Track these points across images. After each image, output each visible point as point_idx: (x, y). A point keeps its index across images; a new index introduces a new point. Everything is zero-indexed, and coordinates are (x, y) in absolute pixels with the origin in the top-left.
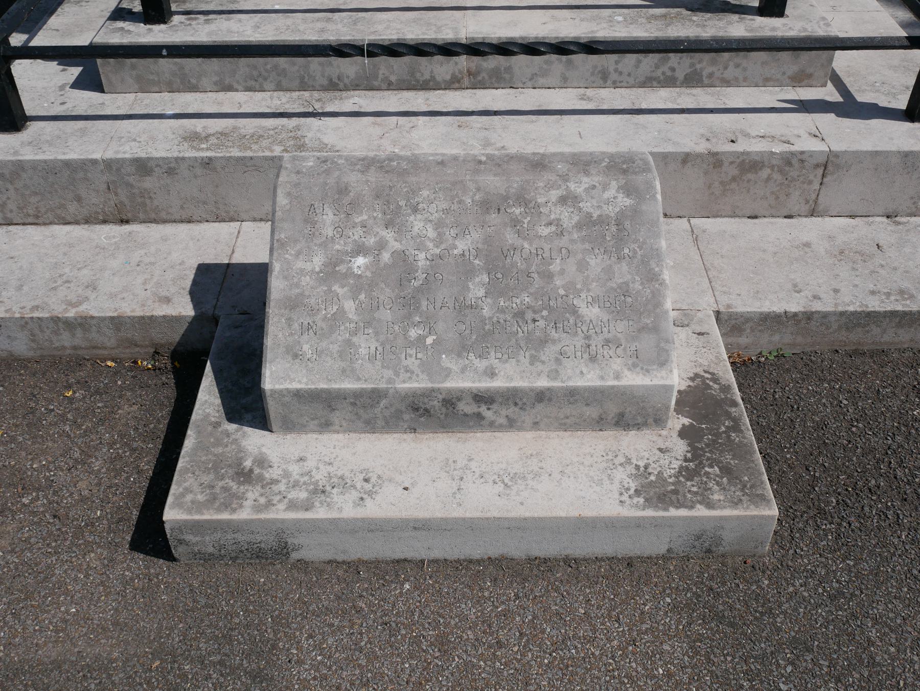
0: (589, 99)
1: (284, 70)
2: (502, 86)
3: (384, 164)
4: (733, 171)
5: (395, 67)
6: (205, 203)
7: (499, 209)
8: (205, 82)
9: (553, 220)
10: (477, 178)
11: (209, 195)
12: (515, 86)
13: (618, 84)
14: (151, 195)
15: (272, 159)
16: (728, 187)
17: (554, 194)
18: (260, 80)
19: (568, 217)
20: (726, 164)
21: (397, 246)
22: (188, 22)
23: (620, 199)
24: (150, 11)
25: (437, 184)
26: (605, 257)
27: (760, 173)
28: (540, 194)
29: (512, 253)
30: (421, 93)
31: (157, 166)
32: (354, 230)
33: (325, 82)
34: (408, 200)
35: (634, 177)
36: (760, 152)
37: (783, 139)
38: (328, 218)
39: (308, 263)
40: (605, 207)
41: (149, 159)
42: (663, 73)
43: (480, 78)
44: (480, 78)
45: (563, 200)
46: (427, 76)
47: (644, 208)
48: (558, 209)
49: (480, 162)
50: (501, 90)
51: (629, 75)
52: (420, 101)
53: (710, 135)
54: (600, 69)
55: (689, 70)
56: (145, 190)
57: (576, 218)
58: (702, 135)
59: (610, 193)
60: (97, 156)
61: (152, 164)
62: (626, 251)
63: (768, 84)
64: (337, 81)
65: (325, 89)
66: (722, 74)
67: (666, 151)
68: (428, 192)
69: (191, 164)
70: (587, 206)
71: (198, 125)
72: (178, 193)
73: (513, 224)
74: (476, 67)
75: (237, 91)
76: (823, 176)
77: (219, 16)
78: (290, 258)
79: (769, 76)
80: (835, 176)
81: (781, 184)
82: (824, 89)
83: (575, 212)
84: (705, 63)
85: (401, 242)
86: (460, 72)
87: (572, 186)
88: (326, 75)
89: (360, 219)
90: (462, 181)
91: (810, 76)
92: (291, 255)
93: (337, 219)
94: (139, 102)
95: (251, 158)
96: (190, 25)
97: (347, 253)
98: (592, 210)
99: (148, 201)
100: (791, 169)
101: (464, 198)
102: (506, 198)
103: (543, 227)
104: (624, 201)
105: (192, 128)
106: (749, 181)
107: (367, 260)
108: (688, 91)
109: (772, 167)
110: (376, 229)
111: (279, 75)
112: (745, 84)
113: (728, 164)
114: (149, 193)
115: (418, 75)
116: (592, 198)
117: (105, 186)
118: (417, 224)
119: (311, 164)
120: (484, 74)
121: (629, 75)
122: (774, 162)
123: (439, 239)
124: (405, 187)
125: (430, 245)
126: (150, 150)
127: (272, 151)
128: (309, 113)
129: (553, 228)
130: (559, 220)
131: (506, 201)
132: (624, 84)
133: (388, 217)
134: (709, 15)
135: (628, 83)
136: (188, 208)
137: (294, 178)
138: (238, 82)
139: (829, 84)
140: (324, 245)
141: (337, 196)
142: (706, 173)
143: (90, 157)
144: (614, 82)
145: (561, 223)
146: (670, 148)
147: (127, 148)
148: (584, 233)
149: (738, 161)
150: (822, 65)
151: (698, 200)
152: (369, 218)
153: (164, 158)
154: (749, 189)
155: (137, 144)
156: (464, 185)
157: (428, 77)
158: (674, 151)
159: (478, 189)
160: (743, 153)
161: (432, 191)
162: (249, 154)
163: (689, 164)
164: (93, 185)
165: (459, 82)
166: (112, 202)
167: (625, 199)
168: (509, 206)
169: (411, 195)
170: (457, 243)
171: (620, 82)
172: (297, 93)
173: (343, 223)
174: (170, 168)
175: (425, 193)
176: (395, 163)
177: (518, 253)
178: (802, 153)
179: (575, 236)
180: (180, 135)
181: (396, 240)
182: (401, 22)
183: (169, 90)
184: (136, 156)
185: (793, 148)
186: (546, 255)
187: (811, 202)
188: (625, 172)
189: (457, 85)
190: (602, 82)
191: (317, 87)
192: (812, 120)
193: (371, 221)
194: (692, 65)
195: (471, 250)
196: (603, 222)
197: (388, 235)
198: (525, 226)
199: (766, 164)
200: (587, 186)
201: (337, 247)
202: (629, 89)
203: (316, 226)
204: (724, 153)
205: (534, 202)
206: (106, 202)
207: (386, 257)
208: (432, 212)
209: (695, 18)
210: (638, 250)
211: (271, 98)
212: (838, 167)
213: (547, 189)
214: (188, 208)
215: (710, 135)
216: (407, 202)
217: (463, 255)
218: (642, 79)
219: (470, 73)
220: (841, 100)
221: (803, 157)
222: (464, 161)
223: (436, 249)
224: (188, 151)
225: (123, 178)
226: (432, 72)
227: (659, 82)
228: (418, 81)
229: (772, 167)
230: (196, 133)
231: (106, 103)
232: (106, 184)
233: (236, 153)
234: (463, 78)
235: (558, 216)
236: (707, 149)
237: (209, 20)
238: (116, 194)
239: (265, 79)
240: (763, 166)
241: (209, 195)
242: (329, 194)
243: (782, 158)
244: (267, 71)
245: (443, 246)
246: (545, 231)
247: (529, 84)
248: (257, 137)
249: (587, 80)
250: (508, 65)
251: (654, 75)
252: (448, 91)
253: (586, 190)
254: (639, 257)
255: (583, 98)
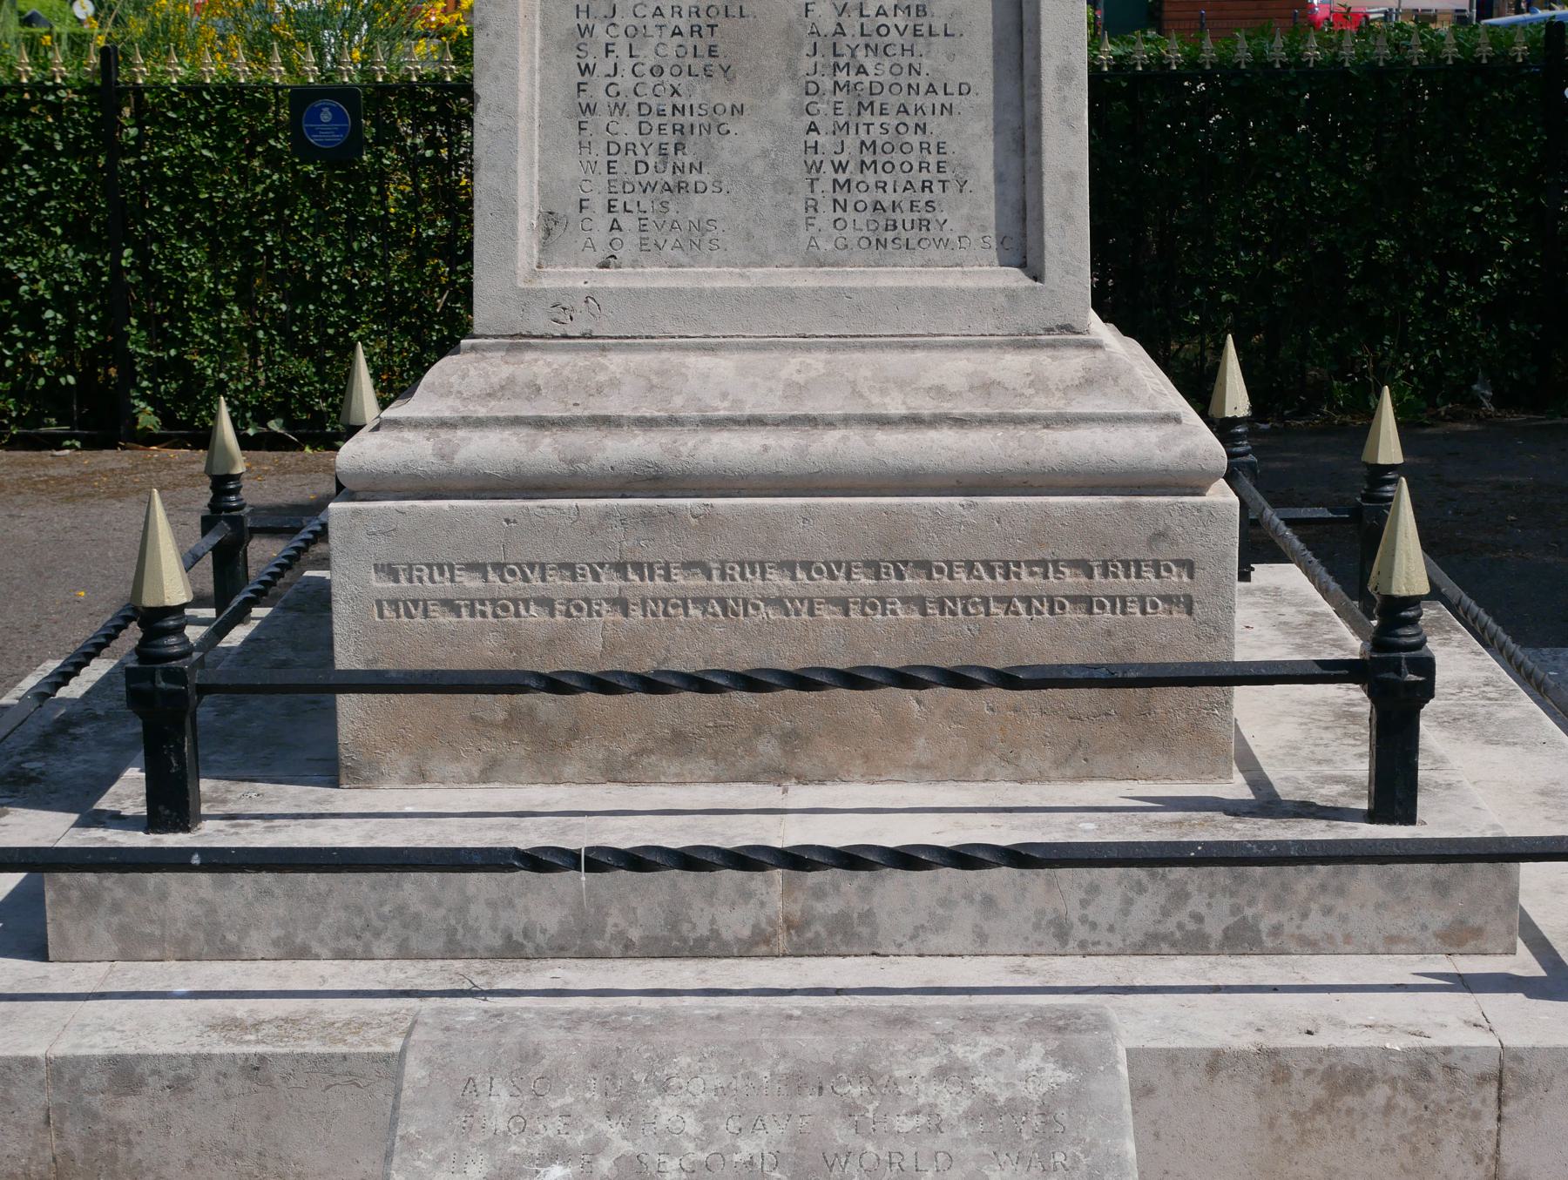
0: (1030, 972)
1: (417, 916)
2: (855, 950)
3: (610, 1019)
4: (1317, 1092)
5: (638, 911)
6: (238, 1155)
7: (821, 1088)
8: (255, 940)
9: (923, 1105)
10: (781, 1036)
11: (250, 1137)
12: (881, 952)
13: (1091, 949)
14: (132, 1137)
15: (386, 1059)
16: (1308, 1125)
17: (926, 1064)
18: (367, 935)
19: (950, 1101)
20: (1298, 1074)
21: (627, 1147)
22: (233, 830)
23: (1048, 1073)
24: (161, 808)
25: (707, 1045)
26: (1019, 1167)
27: (1369, 1095)
28: (899, 1063)
29: (843, 1160)
30: (691, 963)
31: (155, 1072)
32: (547, 1122)
33: (497, 941)
34: (651, 1072)
35: (1076, 1036)
36: (1363, 1049)
37: (1411, 1029)
38: (499, 1102)
39: (458, 1176)
40: (1020, 1086)
41: (140, 1058)
42: (1180, 926)
43: (810, 935)
44: (810, 935)
45: (942, 1073)
46: (703, 930)
47: (1094, 1086)
48: (933, 1088)
49: (790, 1017)
50: (853, 958)
51: (1111, 929)
52: (687, 974)
53: (1265, 1023)
54: (1050, 916)
55: (1231, 921)
56: (121, 1125)
57: (965, 1104)
58: (1250, 1024)
59: (1033, 1061)
60: (38, 1051)
61: (144, 1068)
62: (1060, 1158)
63: (1395, 948)
64: (521, 939)
65: (497, 955)
66: (1299, 927)
67: (1174, 1046)
68: (689, 1060)
69: (223, 1069)
70: (986, 1083)
71: (241, 1008)
72: (188, 1132)
73: (847, 1111)
74: (803, 911)
75: (317, 957)
76: (1500, 1101)
77: (293, 822)
78: (424, 1166)
79: (1394, 932)
80: (1525, 1101)
81: (1418, 1119)
82: (1511, 958)
83: (964, 1092)
84: (1260, 906)
85: (634, 1140)
86: (771, 922)
87: (959, 1050)
88: (501, 926)
89: (560, 1102)
90: (753, 1042)
91: (1478, 932)
92: (426, 1161)
93: (516, 1102)
94: (119, 974)
95: (345, 1057)
96: (237, 833)
97: (532, 1159)
98: (996, 1091)
99: (122, 1150)
100: (1432, 1086)
101: (755, 1069)
102: (834, 1070)
103: (902, 1118)
104: (1055, 1076)
105: (227, 1012)
106: (1350, 1112)
107: (568, 1170)
108: (1234, 960)
109: (1392, 1082)
110: (588, 1119)
111: (405, 926)
112: (1348, 948)
113: (1301, 1075)
114: (127, 1132)
115: (685, 927)
116: (997, 1070)
117: (41, 1116)
118: (666, 1112)
119: (473, 1018)
120: (818, 927)
121: (1111, 929)
122: (1395, 1071)
123: (707, 1136)
124: (647, 1050)
125: (690, 1147)
126: (142, 1043)
127: (386, 1045)
128: (462, 991)
129: (923, 1119)
130: (933, 1106)
131: (835, 1075)
132: (1102, 948)
133: (613, 1099)
134: (1268, 821)
135: (1110, 945)
136: (202, 1166)
137: (440, 1036)
138: (321, 940)
139: (1521, 946)
140: (489, 1145)
141: (517, 1065)
142: (1260, 1094)
143: (23, 1053)
144: (1083, 944)
145: (937, 1111)
146: (1182, 1042)
147: (97, 1039)
148: (980, 1128)
149: (1321, 1068)
150: (1498, 910)
151: (1252, 1155)
152: (577, 1101)
153: (170, 1057)
154: (1353, 1130)
155: (118, 1035)
156: (757, 1049)
157: (706, 933)
158: (1189, 1045)
159: (784, 1055)
160: (1328, 1052)
161: (697, 1058)
162: (340, 1049)
163: (1223, 1074)
164: (17, 1114)
165: (767, 942)
166: (48, 1153)
167: (1059, 1073)
168: (840, 1083)
169: (657, 1065)
170: (740, 1143)
171: (1094, 944)
172: (439, 963)
173: (526, 1109)
174: (179, 1078)
175: (684, 1061)
176: (630, 1018)
177: (854, 1160)
178: (1447, 1051)
179: (964, 1132)
180: (203, 1023)
181: (625, 1138)
182: (655, 831)
183: (179, 956)
184: (115, 1051)
185: (1426, 1043)
186: (908, 1163)
187: (1487, 1160)
188: (1059, 1029)
189: (763, 949)
190: (1057, 944)
191: (481, 952)
192: (1477, 1002)
193: (580, 1107)
194: (1236, 910)
195: (766, 1154)
196: (1016, 1110)
197: (612, 1130)
198: (870, 1115)
199: (1379, 1074)
200: (987, 1050)
201: (514, 1148)
202: (1113, 958)
203: (476, 1114)
204: (1290, 1051)
205: (887, 1077)
206: (34, 1151)
207: (605, 1164)
208: (695, 1092)
209: (1238, 826)
210: (1082, 1156)
211: (387, 970)
212: (1526, 1082)
213: (912, 1056)
214: (202, 1166)
215: (1265, 1023)
216: (649, 1074)
217: (751, 1163)
218: (1138, 937)
219: (790, 925)
220: (1541, 973)
221: (1452, 1060)
222: (759, 1015)
223: (699, 1153)
224: (218, 1044)
225: (81, 1098)
226: (713, 921)
227: (1173, 945)
228: (684, 940)
229: (1392, 1082)
230: (235, 1019)
231: (52, 976)
232: (43, 1113)
233: (314, 1047)
234: (775, 934)
235: (931, 1100)
236: (1255, 1044)
237: (516, 344)
238: (60, 1134)
239: (377, 934)
240: (1373, 1079)
241: (250, 1137)
242: (504, 1061)
243: (1409, 1063)
244: (381, 917)
245: (714, 1149)
246: (906, 1124)
247: (910, 947)
248: (358, 1026)
249: (1026, 939)
250: (867, 907)
251: (1161, 929)
252: (744, 960)
253: (987, 1058)
254: (1084, 1168)
255: (1017, 971)
